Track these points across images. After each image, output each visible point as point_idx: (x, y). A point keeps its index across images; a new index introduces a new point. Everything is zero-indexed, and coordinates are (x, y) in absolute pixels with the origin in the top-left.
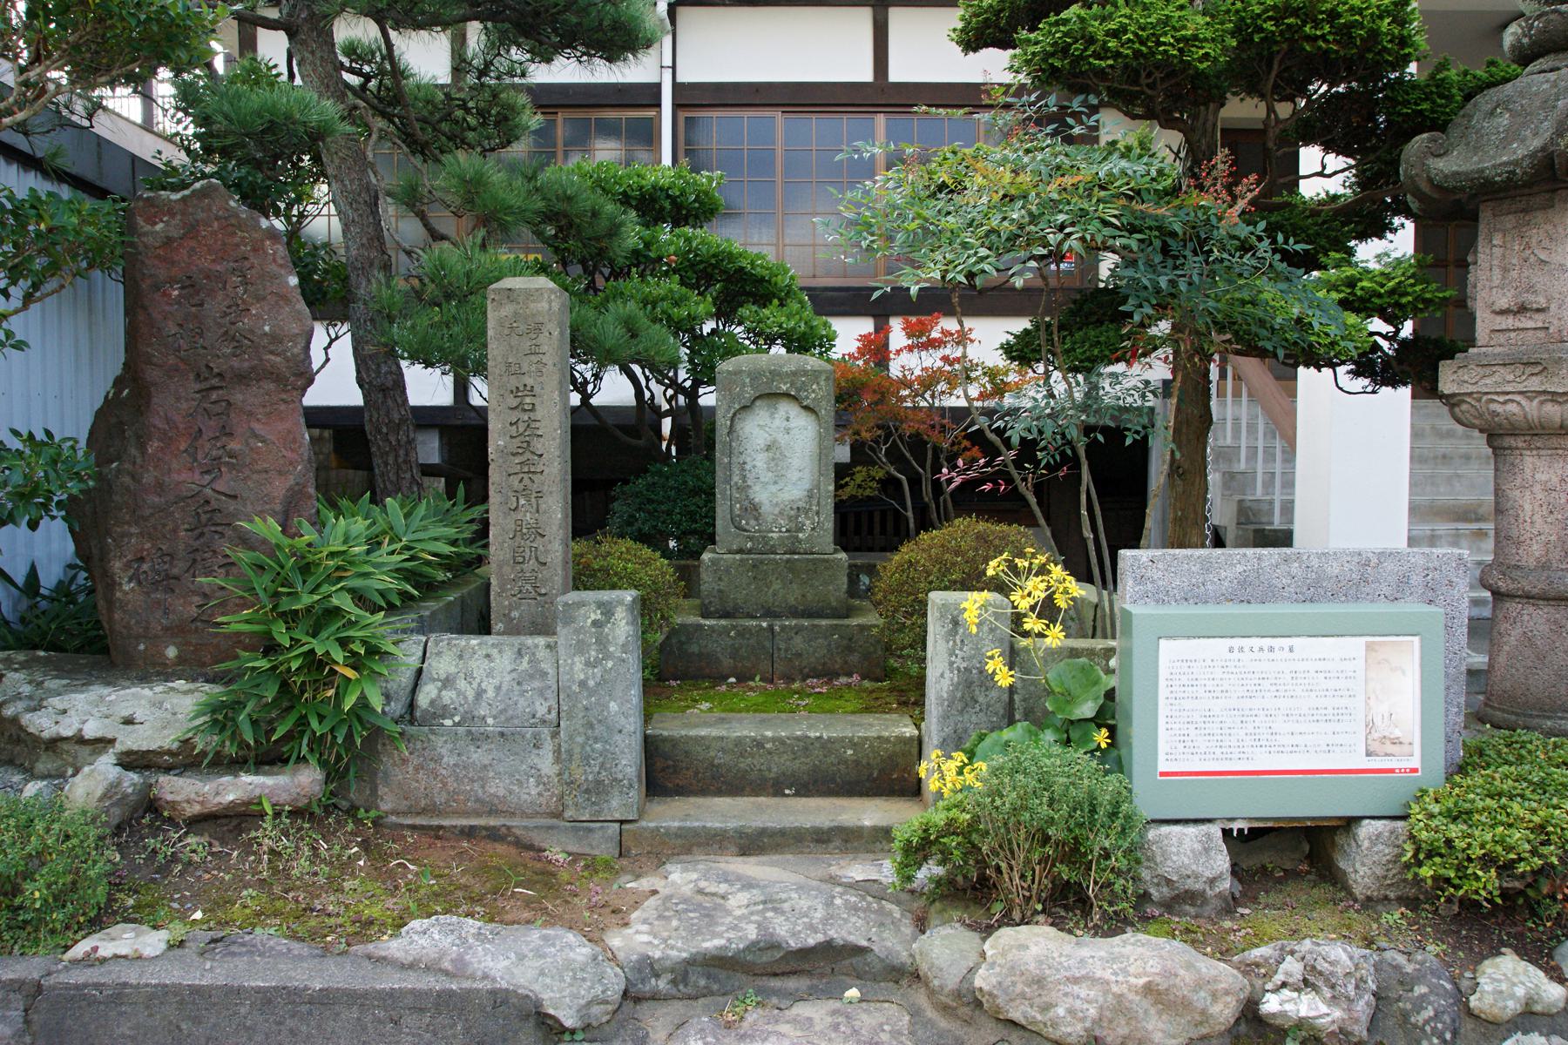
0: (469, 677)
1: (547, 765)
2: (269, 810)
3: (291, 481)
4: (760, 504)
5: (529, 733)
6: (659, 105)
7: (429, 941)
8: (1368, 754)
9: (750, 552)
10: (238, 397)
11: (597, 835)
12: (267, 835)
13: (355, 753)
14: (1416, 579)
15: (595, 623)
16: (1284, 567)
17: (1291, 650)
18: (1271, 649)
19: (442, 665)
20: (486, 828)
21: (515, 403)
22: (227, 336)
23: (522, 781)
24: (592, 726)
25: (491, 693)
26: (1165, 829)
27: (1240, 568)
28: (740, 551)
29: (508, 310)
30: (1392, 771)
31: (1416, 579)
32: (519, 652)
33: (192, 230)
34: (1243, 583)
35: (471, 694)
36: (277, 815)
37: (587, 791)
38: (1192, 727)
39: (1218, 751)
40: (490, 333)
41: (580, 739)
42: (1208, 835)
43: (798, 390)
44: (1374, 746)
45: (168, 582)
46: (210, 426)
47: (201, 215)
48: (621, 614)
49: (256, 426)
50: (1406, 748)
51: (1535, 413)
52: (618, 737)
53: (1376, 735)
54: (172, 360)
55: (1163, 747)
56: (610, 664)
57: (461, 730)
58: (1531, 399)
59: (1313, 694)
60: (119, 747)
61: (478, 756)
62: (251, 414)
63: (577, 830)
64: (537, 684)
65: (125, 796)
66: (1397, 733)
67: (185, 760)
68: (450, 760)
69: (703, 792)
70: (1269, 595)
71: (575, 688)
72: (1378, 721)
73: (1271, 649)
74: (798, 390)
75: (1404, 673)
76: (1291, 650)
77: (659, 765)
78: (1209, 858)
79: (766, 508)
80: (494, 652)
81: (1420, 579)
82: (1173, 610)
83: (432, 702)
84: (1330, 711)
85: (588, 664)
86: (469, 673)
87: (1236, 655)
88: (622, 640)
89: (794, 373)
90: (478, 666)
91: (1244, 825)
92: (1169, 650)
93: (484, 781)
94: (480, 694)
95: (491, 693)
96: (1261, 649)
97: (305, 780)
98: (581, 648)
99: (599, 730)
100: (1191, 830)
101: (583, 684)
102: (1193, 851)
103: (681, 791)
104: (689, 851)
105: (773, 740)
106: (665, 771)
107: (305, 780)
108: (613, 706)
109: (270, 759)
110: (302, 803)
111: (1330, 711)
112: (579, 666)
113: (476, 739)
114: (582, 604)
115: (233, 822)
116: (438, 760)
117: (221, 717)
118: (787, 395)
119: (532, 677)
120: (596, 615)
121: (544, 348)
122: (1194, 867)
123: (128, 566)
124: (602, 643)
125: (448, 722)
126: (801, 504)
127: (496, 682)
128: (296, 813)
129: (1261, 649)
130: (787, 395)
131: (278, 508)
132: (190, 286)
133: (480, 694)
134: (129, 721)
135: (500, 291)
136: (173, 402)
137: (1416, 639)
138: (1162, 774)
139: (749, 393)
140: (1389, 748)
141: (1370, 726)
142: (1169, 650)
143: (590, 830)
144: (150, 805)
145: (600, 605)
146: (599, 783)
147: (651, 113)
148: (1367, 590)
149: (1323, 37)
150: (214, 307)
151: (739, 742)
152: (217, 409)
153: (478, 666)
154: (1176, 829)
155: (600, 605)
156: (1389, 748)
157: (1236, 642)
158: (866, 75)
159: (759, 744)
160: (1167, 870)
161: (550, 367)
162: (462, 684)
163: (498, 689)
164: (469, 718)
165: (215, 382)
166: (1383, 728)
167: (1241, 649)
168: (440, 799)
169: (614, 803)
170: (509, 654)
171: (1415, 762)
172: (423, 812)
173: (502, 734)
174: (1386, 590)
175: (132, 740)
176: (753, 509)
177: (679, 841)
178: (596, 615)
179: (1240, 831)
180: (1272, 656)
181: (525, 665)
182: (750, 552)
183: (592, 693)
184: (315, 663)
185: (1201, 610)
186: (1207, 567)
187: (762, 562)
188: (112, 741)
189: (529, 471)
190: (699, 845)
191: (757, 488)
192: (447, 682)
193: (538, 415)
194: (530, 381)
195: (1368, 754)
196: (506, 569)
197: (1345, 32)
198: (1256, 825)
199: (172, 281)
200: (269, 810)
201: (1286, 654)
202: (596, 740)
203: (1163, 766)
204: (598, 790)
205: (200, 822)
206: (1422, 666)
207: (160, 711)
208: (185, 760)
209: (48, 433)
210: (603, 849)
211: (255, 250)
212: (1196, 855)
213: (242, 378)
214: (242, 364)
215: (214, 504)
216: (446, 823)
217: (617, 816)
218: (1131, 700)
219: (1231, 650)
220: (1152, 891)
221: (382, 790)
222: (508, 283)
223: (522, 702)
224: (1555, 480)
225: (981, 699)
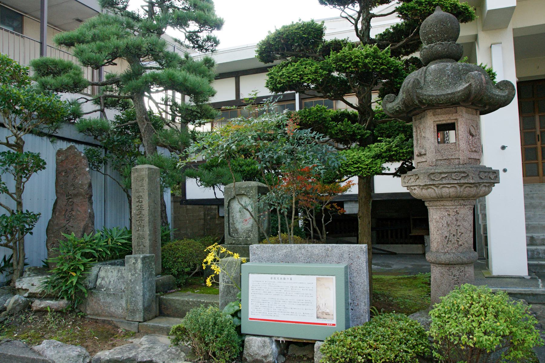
0: (108, 277)
2: (49, 310)
3: (85, 222)
4: (238, 229)
5: (120, 294)
6: (295, 99)
8: (318, 318)
9: (234, 244)
10: (75, 200)
11: (133, 325)
12: (48, 317)
14: (346, 256)
15: (133, 263)
16: (299, 251)
17: (291, 279)
18: (284, 279)
19: (102, 274)
20: (108, 321)
21: (138, 200)
22: (73, 185)
23: (117, 308)
24: (132, 293)
25: (112, 282)
26: (251, 337)
27: (285, 251)
28: (231, 244)
29: (136, 174)
30: (326, 324)
31: (346, 256)
32: (118, 271)
33: (67, 158)
34: (286, 256)
35: (108, 282)
36: (51, 311)
37: (131, 312)
38: (259, 304)
39: (268, 312)
40: (132, 181)
41: (130, 297)
42: (265, 342)
43: (247, 193)
44: (320, 315)
46: (69, 208)
47: (69, 154)
48: (139, 261)
49: (78, 208)
50: (331, 316)
51: (439, 192)
52: (138, 297)
53: (320, 311)
54: (62, 191)
55: (250, 310)
56: (137, 275)
57: (105, 292)
58: (437, 187)
59: (298, 295)
60: (29, 292)
61: (109, 300)
62: (77, 205)
63: (128, 323)
64: (122, 280)
65: (20, 304)
66: (328, 311)
67: (42, 296)
68: (102, 300)
69: (174, 316)
70: (295, 260)
71: (129, 282)
72: (321, 306)
73: (284, 279)
74: (247, 193)
75: (330, 289)
76: (291, 279)
77: (163, 306)
78: (264, 349)
79: (240, 230)
80: (113, 270)
81: (347, 255)
82: (264, 264)
83: (100, 284)
84: (304, 301)
85: (132, 275)
87: (273, 280)
88: (139, 268)
89: (246, 188)
90: (110, 274)
91: (284, 340)
92: (253, 278)
93: (109, 307)
94: (110, 282)
95: (112, 282)
96: (281, 279)
97: (62, 303)
98: (130, 270)
99: (134, 294)
100: (259, 339)
101: (130, 280)
102: (258, 346)
103: (168, 316)
104: (155, 333)
105: (192, 301)
107: (62, 303)
108: (137, 287)
110: (60, 309)
111: (304, 301)
112: (130, 276)
113: (109, 295)
114: (131, 258)
115: (42, 312)
116: (100, 300)
118: (243, 194)
119: (121, 278)
120: (134, 261)
121: (144, 185)
122: (258, 351)
123: (51, 245)
124: (135, 269)
125: (103, 290)
126: (250, 229)
127: (113, 279)
128: (57, 311)
129: (281, 279)
130: (243, 194)
131: (82, 230)
133: (110, 282)
134: (33, 285)
135: (134, 169)
137: (334, 277)
138: (250, 319)
139: (233, 194)
140: (325, 316)
141: (318, 308)
142: (253, 278)
143: (131, 324)
145: (135, 258)
146: (134, 310)
147: (292, 102)
148: (328, 259)
149: (350, 67)
150: (71, 177)
151: (183, 301)
152: (71, 204)
153: (110, 274)
154: (255, 338)
155: (135, 258)
156: (325, 316)
157: (273, 276)
158: (234, 98)
159: (188, 303)
160: (250, 351)
161: (146, 190)
162: (106, 279)
163: (114, 281)
164: (108, 289)
165: (70, 197)
166: (323, 309)
167: (275, 278)
168: (100, 311)
169: (137, 316)
170: (116, 271)
171: (334, 322)
172: (96, 315)
173: (114, 294)
174: (335, 259)
176: (236, 230)
177: (152, 329)
178: (134, 261)
179: (282, 341)
180: (285, 281)
181: (120, 275)
182: (234, 244)
183: (133, 283)
185: (273, 265)
186: (274, 250)
187: (235, 247)
188: (28, 290)
189: (141, 219)
190: (157, 331)
191: (237, 224)
192: (103, 279)
193: (143, 203)
194: (141, 194)
195: (318, 318)
196: (136, 248)
197: (356, 64)
198: (289, 340)
199: (63, 171)
200: (49, 310)
201: (289, 280)
202: (133, 297)
203: (250, 316)
204: (133, 312)
206: (336, 287)
209: (27, 211)
210: (134, 330)
211: (80, 162)
212: (259, 348)
213: (76, 195)
214: (75, 192)
215: (68, 229)
216: (99, 318)
217: (138, 320)
219: (272, 278)
220: (247, 358)
221: (88, 308)
222: (137, 167)
223: (119, 285)
224: (438, 218)
225: (232, 292)
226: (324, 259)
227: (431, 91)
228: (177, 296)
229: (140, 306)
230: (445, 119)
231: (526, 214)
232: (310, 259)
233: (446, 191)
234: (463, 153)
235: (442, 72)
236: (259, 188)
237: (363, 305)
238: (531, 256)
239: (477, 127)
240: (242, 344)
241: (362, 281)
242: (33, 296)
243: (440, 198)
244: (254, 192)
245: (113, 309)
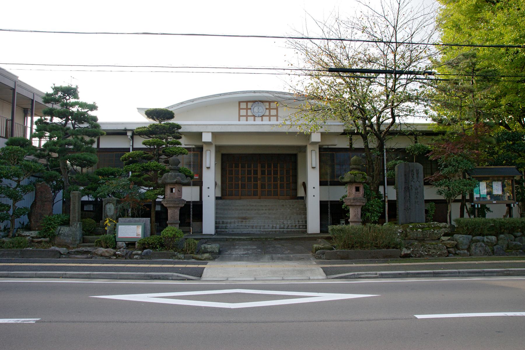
1: (71, 239)
7: (53, 248)
12: (43, 243)
13: (53, 237)
19: (62, 229)
45: (37, 222)
61: (65, 238)
67: (37, 237)
86: (65, 230)
92: (120, 226)
106: (84, 241)
107: (48, 239)
109: (45, 237)
113: (65, 236)
117: (40, 233)
132: (41, 192)
136: (39, 203)
142: (120, 226)
144: (33, 241)
175: (32, 236)
184: (49, 228)
204: (75, 241)
205: (38, 242)
207: (34, 233)
208: (37, 237)
213: (46, 201)
218: (262, 262)
226: (139, 221)
227: (168, 181)
228: (266, 96)
229: (78, 239)
230: (172, 187)
231: (216, 213)
232: (135, 222)
233: (171, 205)
234: (176, 195)
235: (171, 175)
236: (117, 200)
237: (149, 233)
238: (216, 228)
239: (181, 189)
240: (116, 244)
241: (149, 227)
242: (33, 237)
243: (170, 207)
244: (115, 202)
245: (66, 241)
